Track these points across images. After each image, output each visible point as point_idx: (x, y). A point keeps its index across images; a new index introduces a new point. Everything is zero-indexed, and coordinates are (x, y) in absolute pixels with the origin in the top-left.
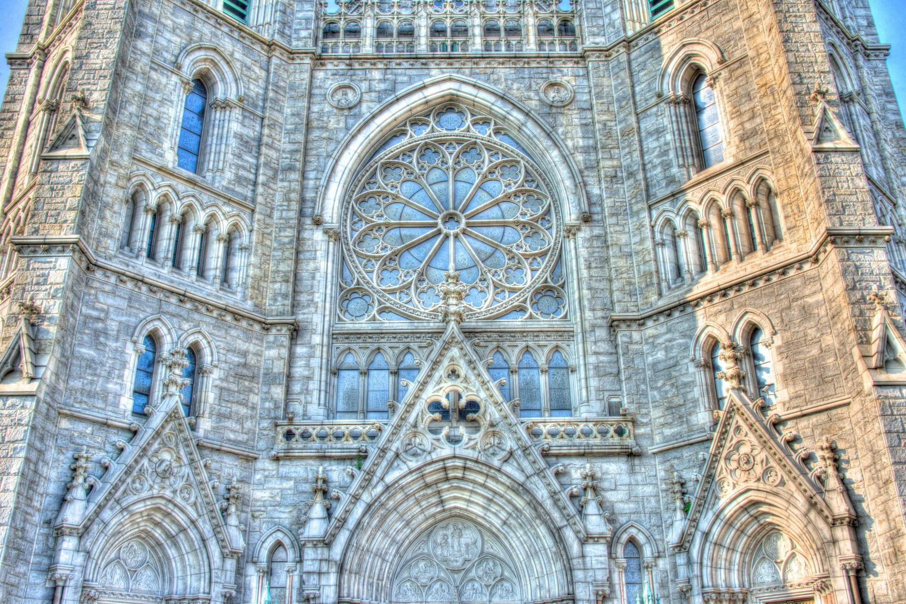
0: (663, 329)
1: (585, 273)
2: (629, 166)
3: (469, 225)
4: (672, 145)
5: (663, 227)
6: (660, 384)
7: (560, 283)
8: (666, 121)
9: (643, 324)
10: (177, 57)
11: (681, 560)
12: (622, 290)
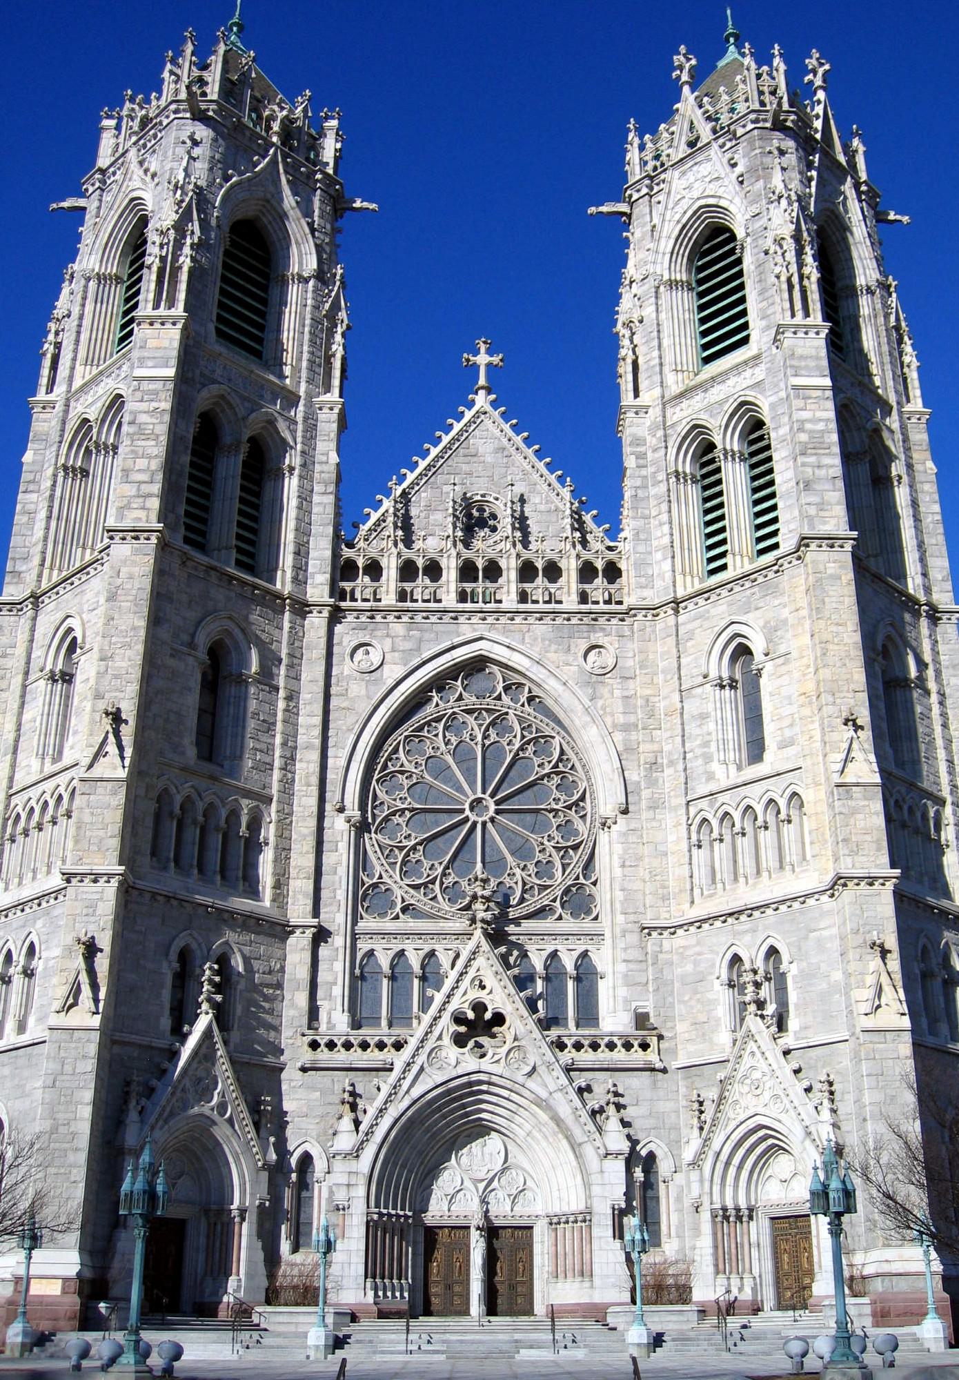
0: (693, 941)
1: (618, 872)
2: (670, 753)
3: (497, 803)
4: (714, 737)
5: (700, 826)
6: (686, 998)
7: (593, 879)
8: (711, 706)
9: (674, 933)
10: (193, 636)
11: (694, 1175)
12: (654, 894)
